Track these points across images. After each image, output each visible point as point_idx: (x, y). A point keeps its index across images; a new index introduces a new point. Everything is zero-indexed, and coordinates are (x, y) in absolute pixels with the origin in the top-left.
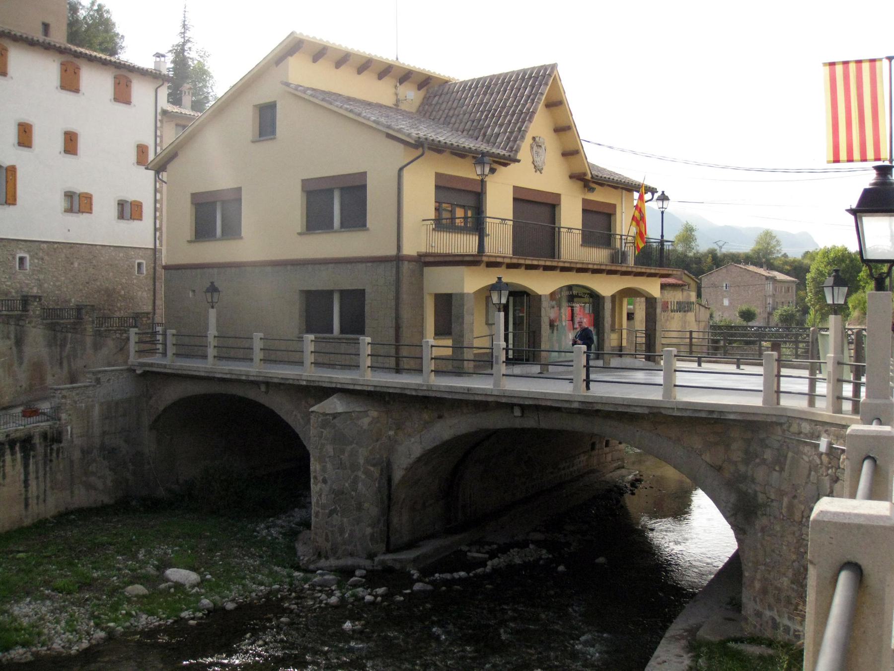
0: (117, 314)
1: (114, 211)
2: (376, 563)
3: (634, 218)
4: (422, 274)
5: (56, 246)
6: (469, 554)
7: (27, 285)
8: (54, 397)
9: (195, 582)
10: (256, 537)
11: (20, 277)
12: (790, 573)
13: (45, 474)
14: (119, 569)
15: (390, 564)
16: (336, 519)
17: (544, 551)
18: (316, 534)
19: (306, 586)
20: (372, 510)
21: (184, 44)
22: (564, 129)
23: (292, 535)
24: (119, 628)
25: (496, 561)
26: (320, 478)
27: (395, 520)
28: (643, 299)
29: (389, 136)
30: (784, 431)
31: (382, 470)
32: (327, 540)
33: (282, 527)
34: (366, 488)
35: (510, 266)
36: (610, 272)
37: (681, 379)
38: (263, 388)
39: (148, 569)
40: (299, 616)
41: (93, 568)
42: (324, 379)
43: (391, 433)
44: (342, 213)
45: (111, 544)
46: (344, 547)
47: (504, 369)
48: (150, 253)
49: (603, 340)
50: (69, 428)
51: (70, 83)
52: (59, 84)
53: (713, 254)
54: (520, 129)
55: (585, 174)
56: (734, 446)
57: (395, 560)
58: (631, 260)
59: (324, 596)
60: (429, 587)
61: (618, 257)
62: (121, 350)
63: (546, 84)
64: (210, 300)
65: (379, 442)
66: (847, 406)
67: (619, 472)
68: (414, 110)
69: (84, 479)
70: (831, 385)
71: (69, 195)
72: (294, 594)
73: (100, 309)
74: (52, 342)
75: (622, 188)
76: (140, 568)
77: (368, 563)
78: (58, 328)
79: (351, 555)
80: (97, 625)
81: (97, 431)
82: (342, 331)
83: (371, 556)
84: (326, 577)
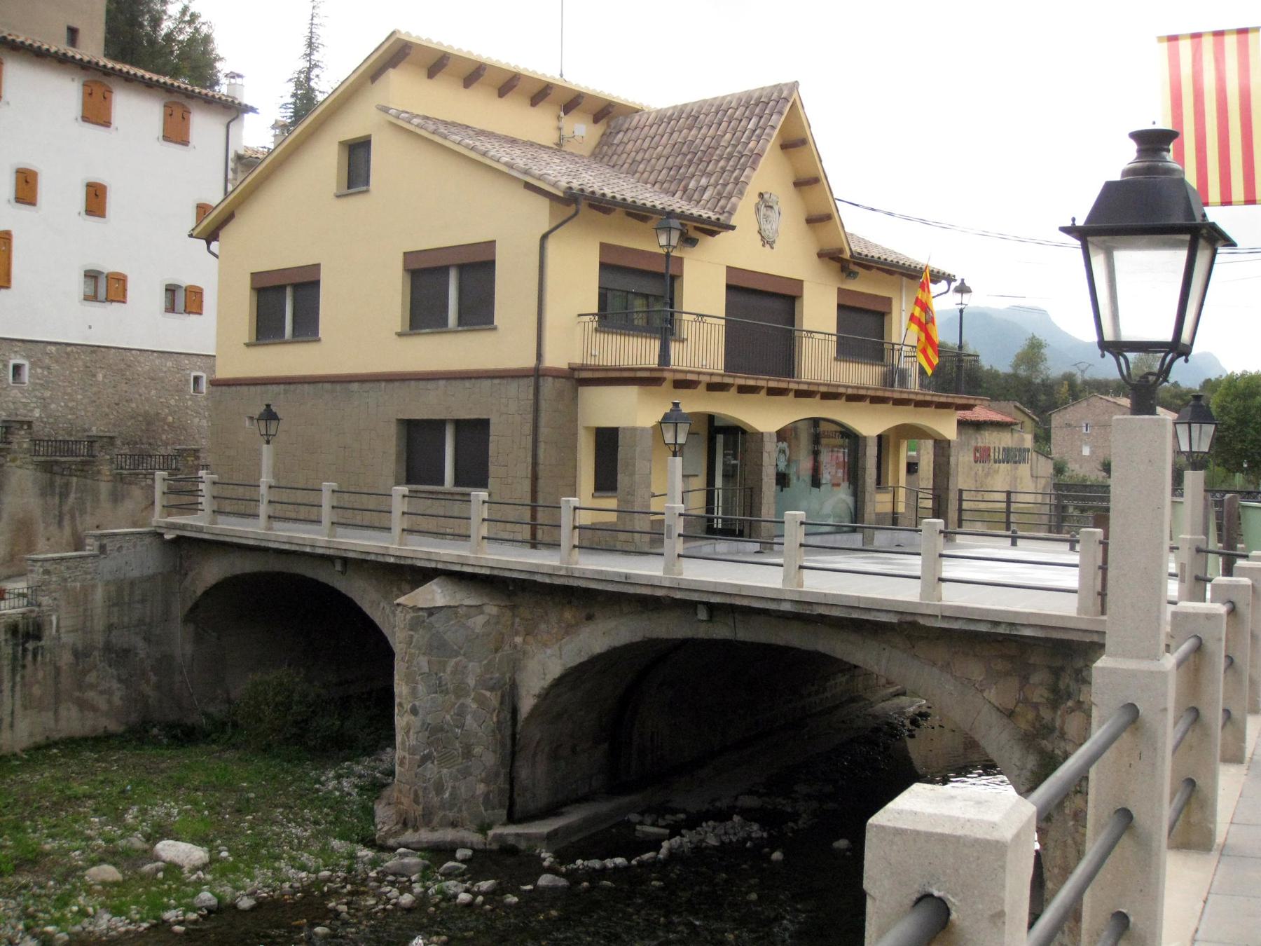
0: (162, 451)
1: (160, 299)
2: (489, 838)
3: (913, 318)
4: (575, 398)
5: (69, 349)
6: (638, 827)
7: (25, 405)
8: (32, 571)
9: (198, 863)
10: (318, 791)
13: (13, 687)
14: (90, 838)
15: (511, 841)
16: (431, 769)
17: (755, 827)
18: (400, 791)
19: (373, 874)
20: (486, 756)
21: (310, 69)
22: (809, 182)
23: (375, 788)
24: (62, 935)
25: (676, 841)
26: (408, 706)
27: (524, 773)
28: (930, 443)
29: (528, 186)
31: (503, 696)
32: (416, 801)
33: (361, 776)
34: (479, 723)
35: (712, 387)
36: (876, 400)
37: (950, 569)
38: (338, 567)
39: (133, 840)
40: (345, 924)
41: (48, 836)
42: (420, 556)
45: (90, 797)
46: (441, 814)
47: (680, 546)
49: (864, 502)
50: (54, 619)
51: (96, 113)
52: (80, 114)
53: (1069, 379)
55: (841, 251)
56: (1035, 678)
57: (518, 835)
58: (914, 384)
59: (395, 892)
60: (562, 882)
61: (893, 377)
63: (781, 113)
64: (264, 432)
65: (499, 654)
67: (896, 701)
68: (587, 154)
69: (77, 694)
70: (1186, 584)
71: (92, 276)
72: (349, 887)
73: (136, 443)
74: (46, 491)
75: (903, 274)
76: (122, 837)
77: (476, 838)
78: (55, 468)
79: (454, 825)
80: (28, 929)
81: (99, 624)
82: (457, 482)
83: (483, 829)
84: (406, 860)
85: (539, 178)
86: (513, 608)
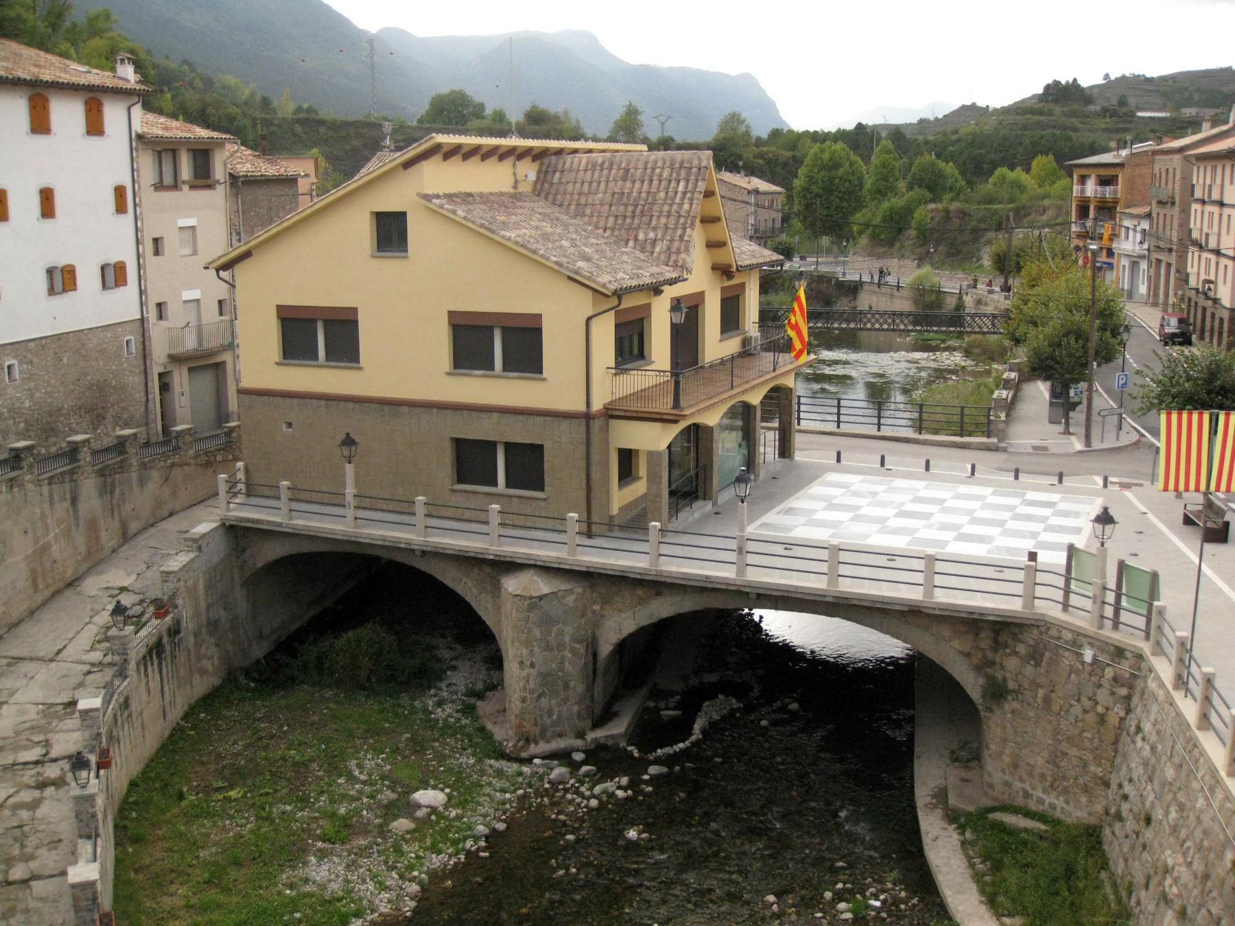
7: (19, 399)
11: (10, 390)
12: (1046, 754)
15: (602, 741)
17: (734, 701)
29: (570, 278)
30: (1041, 633)
32: (536, 724)
34: (572, 666)
43: (597, 607)
44: (503, 350)
48: (138, 324)
51: (40, 124)
54: (681, 237)
56: (983, 635)
62: (166, 480)
66: (1109, 624)
77: (579, 743)
78: (107, 472)
79: (560, 736)
83: (581, 735)
85: (589, 278)
86: (591, 587)
